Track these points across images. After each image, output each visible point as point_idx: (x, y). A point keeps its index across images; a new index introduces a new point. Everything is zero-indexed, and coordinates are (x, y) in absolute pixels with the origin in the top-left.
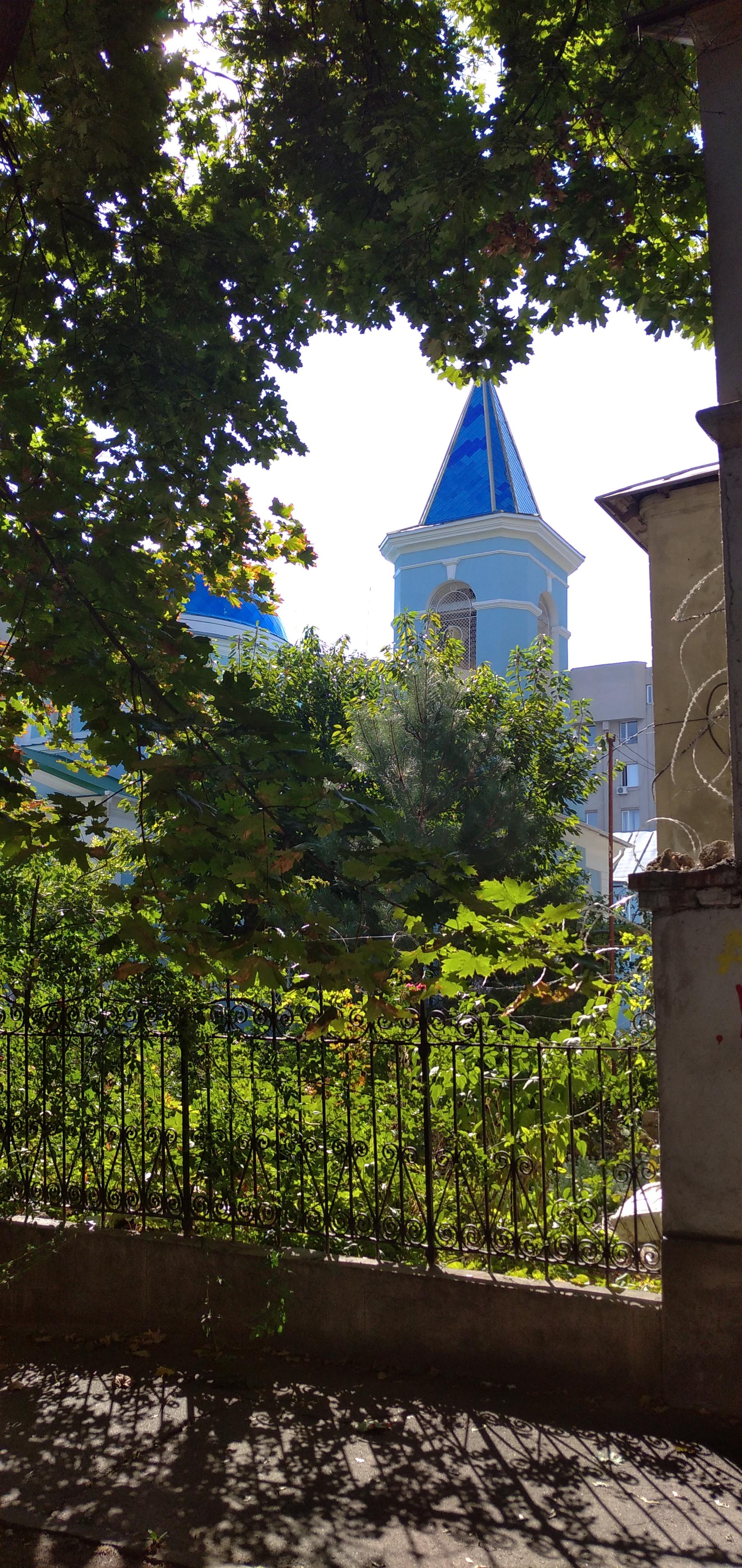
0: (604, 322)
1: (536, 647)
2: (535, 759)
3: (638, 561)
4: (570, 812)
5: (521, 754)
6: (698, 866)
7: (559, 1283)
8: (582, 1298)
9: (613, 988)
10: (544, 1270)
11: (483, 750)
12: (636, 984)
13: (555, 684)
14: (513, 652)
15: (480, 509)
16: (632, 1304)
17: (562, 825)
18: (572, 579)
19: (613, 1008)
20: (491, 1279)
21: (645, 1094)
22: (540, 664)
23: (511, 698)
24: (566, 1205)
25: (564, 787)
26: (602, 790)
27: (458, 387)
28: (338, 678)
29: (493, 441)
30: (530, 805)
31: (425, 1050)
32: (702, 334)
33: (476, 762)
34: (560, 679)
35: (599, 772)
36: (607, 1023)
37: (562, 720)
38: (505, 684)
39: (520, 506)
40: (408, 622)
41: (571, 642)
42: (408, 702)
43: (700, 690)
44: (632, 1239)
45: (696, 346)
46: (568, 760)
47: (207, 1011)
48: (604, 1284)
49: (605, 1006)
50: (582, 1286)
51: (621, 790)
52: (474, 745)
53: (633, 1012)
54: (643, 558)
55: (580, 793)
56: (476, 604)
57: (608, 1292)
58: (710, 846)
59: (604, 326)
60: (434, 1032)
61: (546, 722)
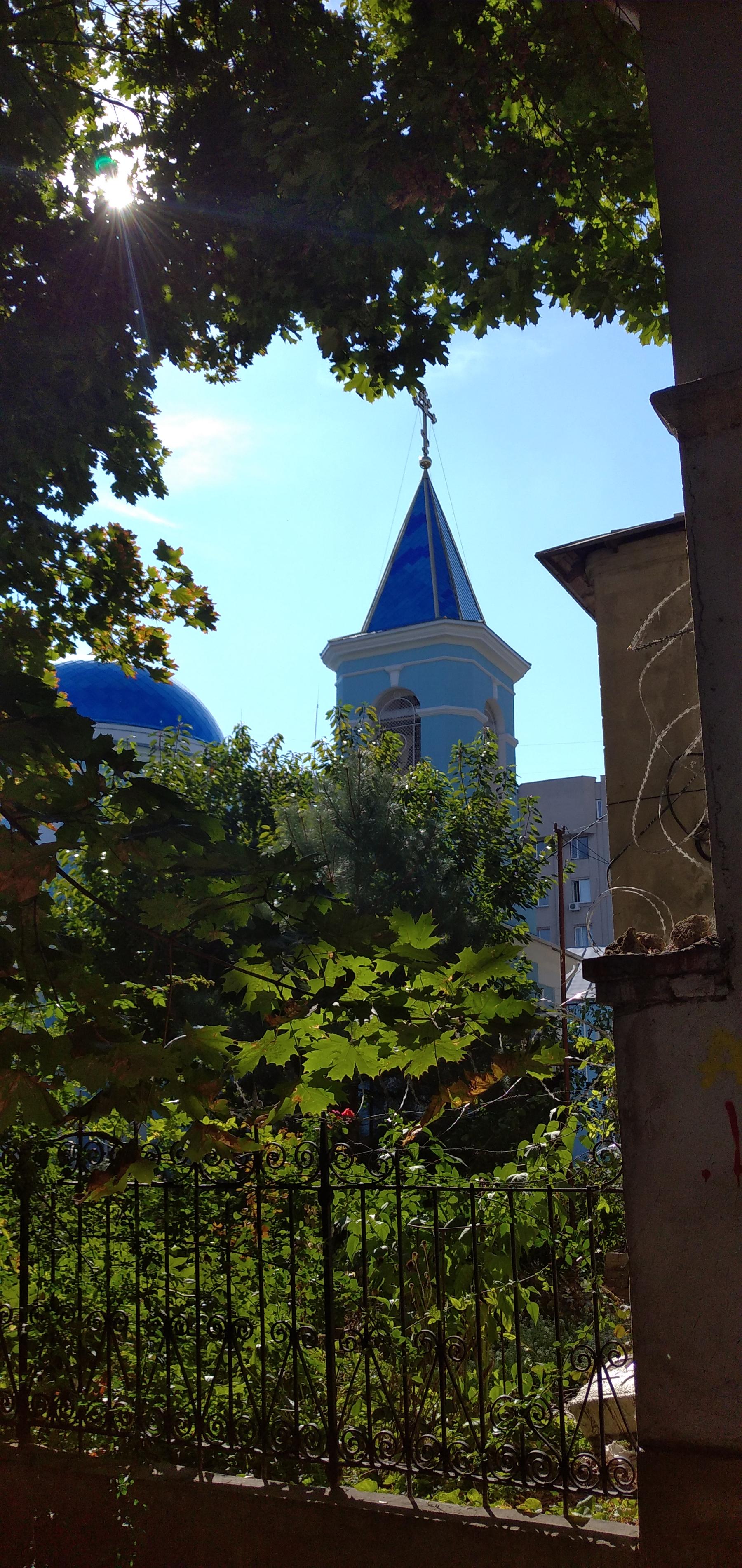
0: (535, 319)
1: (480, 742)
2: (480, 859)
3: (583, 629)
4: (519, 917)
5: (466, 855)
6: (670, 947)
7: (502, 1510)
8: (532, 1533)
9: (567, 1110)
10: (482, 1487)
11: (421, 847)
12: (595, 1103)
13: (500, 780)
14: (455, 748)
15: (423, 615)
16: (599, 1542)
17: (510, 932)
18: (519, 687)
19: (568, 1135)
20: (411, 1507)
21: (607, 1231)
22: (484, 759)
23: (454, 795)
24: (509, 1404)
25: (512, 892)
26: (553, 893)
27: (370, 400)
28: (270, 780)
29: (435, 548)
30: (475, 909)
31: (326, 1195)
32: (651, 327)
33: (413, 860)
34: (505, 774)
35: (547, 873)
36: (561, 1153)
37: (508, 819)
38: (445, 780)
39: (464, 613)
40: (342, 716)
41: (518, 749)
42: (341, 799)
43: (664, 733)
44: (597, 1430)
45: (644, 340)
46: (515, 861)
47: (53, 1150)
48: (561, 1511)
49: (558, 1132)
50: (532, 1515)
51: (573, 906)
52: (411, 842)
53: (592, 1140)
54: (589, 626)
55: (529, 897)
56: (420, 712)
57: (566, 1524)
58: (685, 923)
59: (535, 323)
60: (339, 1172)
61: (492, 820)
